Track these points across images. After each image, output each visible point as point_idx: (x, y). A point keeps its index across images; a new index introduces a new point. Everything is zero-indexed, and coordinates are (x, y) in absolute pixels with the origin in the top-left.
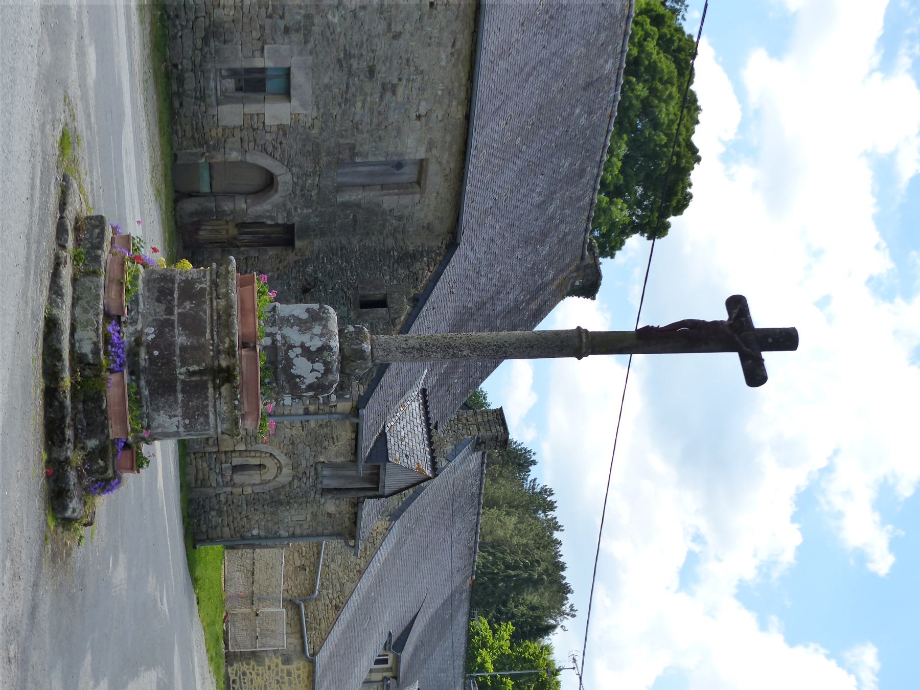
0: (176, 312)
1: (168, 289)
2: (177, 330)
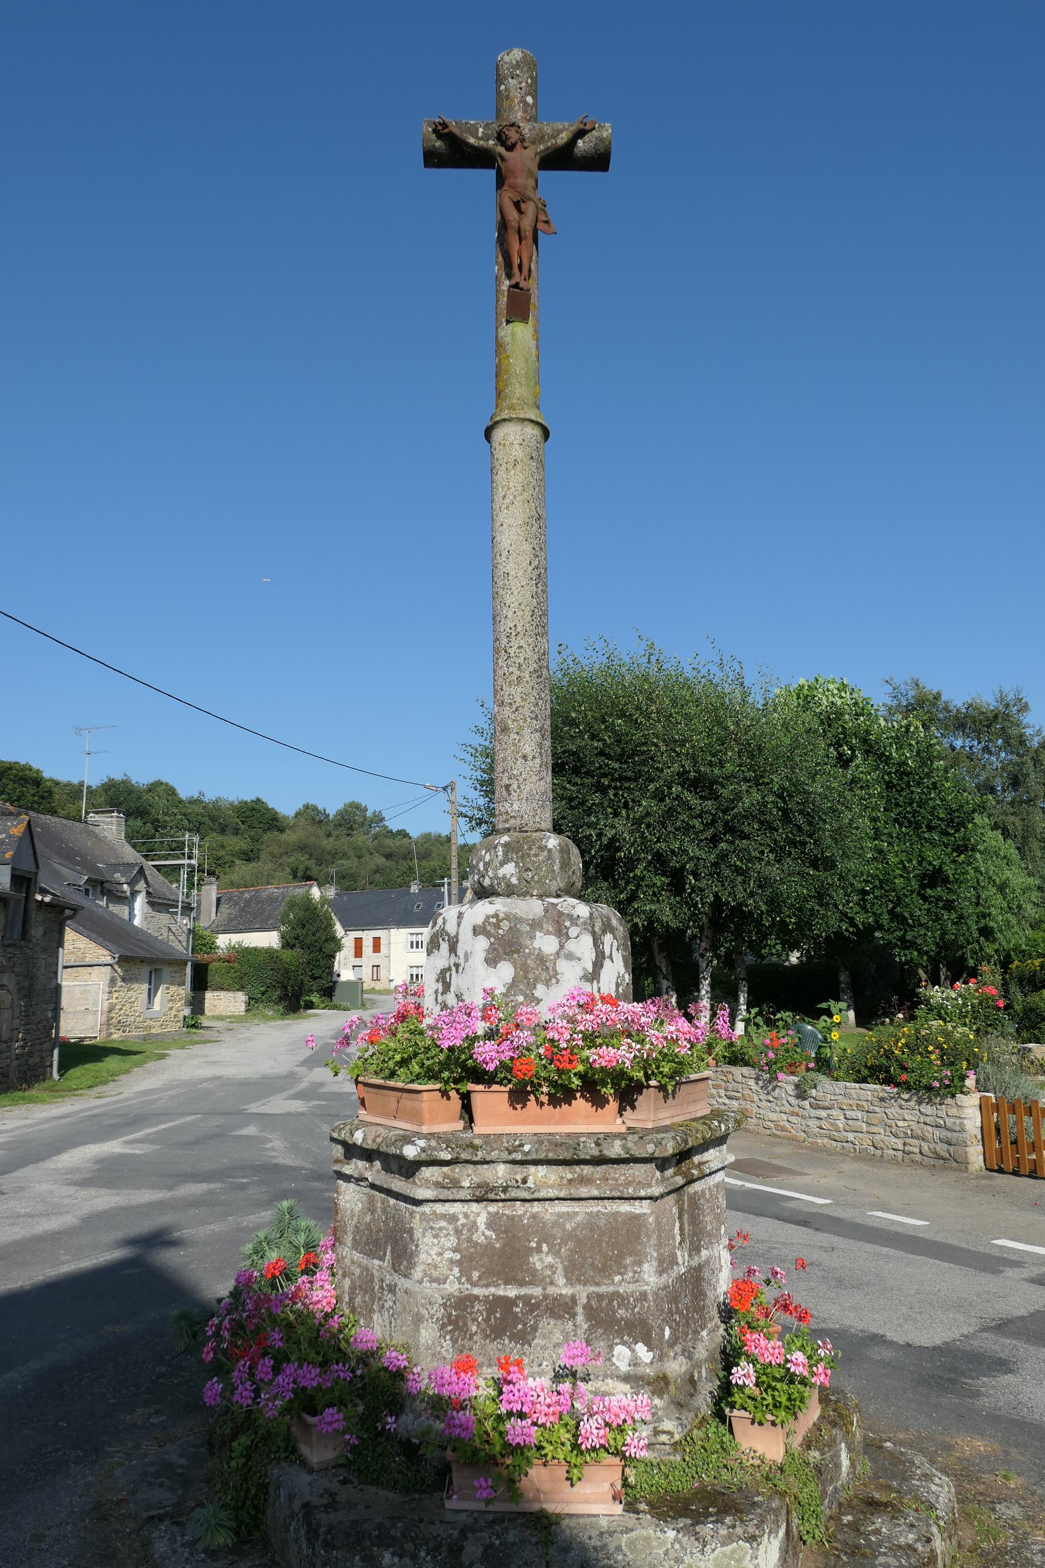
0: (567, 1291)
1: (490, 1311)
2: (620, 1284)
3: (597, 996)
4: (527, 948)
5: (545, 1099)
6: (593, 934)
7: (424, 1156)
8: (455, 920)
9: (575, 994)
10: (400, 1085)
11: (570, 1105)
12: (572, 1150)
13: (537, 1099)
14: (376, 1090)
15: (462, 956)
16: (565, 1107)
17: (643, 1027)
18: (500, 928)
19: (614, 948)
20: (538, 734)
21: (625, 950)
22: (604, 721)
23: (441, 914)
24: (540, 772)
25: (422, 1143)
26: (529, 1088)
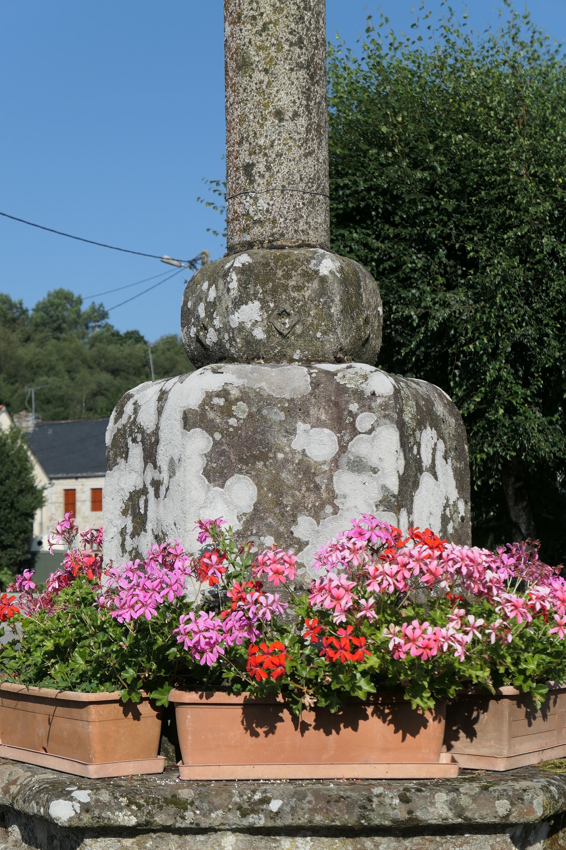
3: (405, 534)
4: (281, 450)
5: (309, 717)
6: (401, 425)
7: (86, 819)
8: (153, 405)
9: (365, 526)
10: (50, 692)
11: (355, 728)
12: (357, 811)
13: (295, 719)
14: (12, 703)
15: (165, 467)
16: (346, 732)
17: (490, 589)
18: (231, 415)
19: (439, 455)
20: (302, 73)
21: (459, 458)
22: (433, 136)
23: (131, 396)
24: (306, 141)
25: (83, 796)
26: (280, 699)
